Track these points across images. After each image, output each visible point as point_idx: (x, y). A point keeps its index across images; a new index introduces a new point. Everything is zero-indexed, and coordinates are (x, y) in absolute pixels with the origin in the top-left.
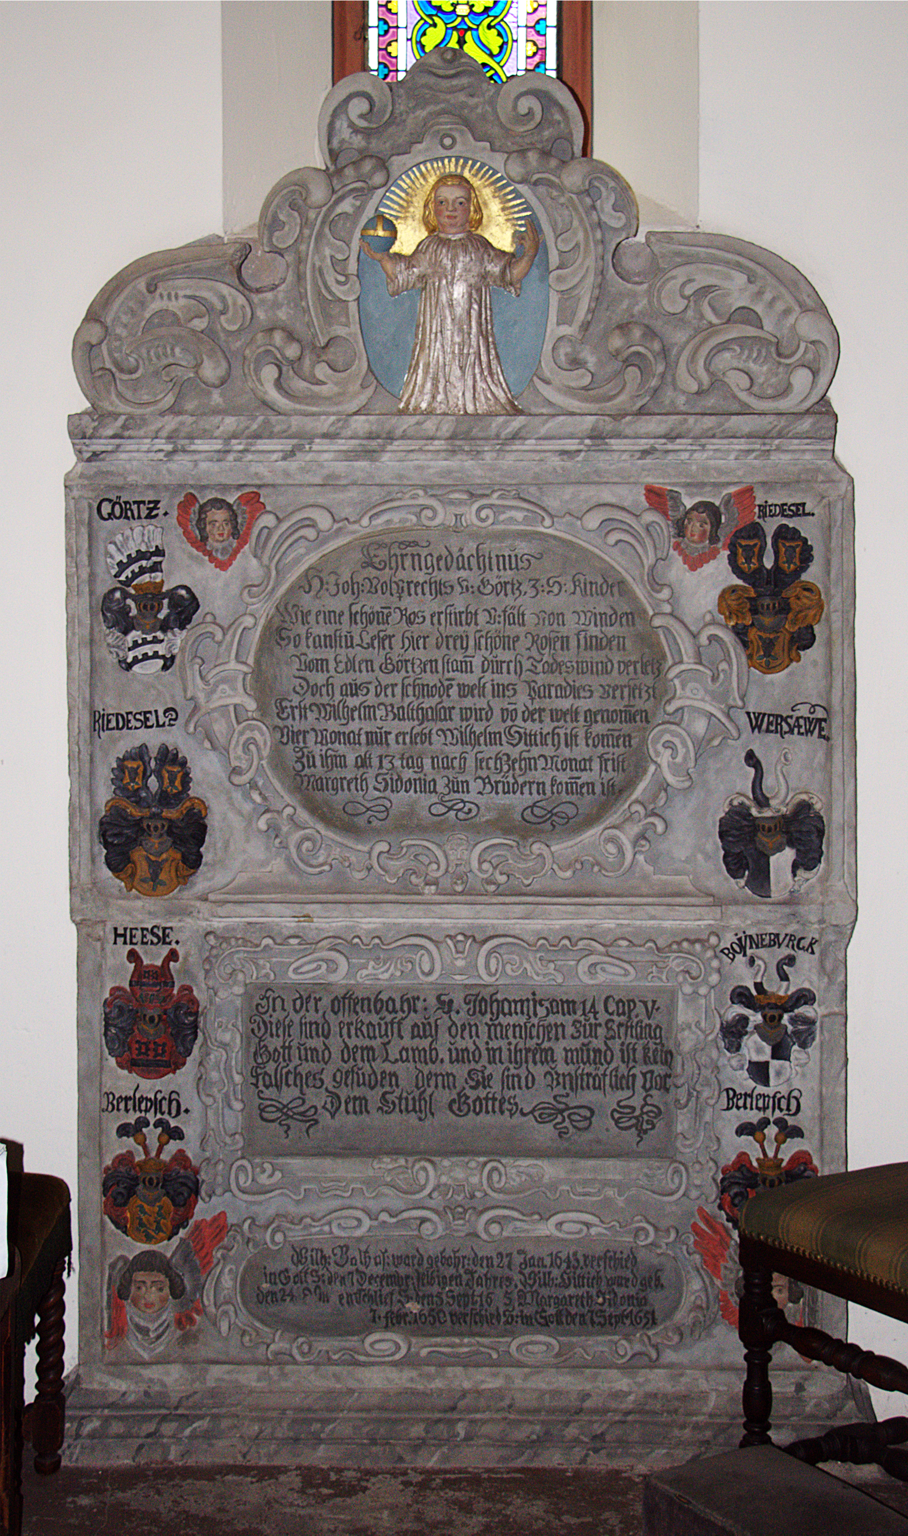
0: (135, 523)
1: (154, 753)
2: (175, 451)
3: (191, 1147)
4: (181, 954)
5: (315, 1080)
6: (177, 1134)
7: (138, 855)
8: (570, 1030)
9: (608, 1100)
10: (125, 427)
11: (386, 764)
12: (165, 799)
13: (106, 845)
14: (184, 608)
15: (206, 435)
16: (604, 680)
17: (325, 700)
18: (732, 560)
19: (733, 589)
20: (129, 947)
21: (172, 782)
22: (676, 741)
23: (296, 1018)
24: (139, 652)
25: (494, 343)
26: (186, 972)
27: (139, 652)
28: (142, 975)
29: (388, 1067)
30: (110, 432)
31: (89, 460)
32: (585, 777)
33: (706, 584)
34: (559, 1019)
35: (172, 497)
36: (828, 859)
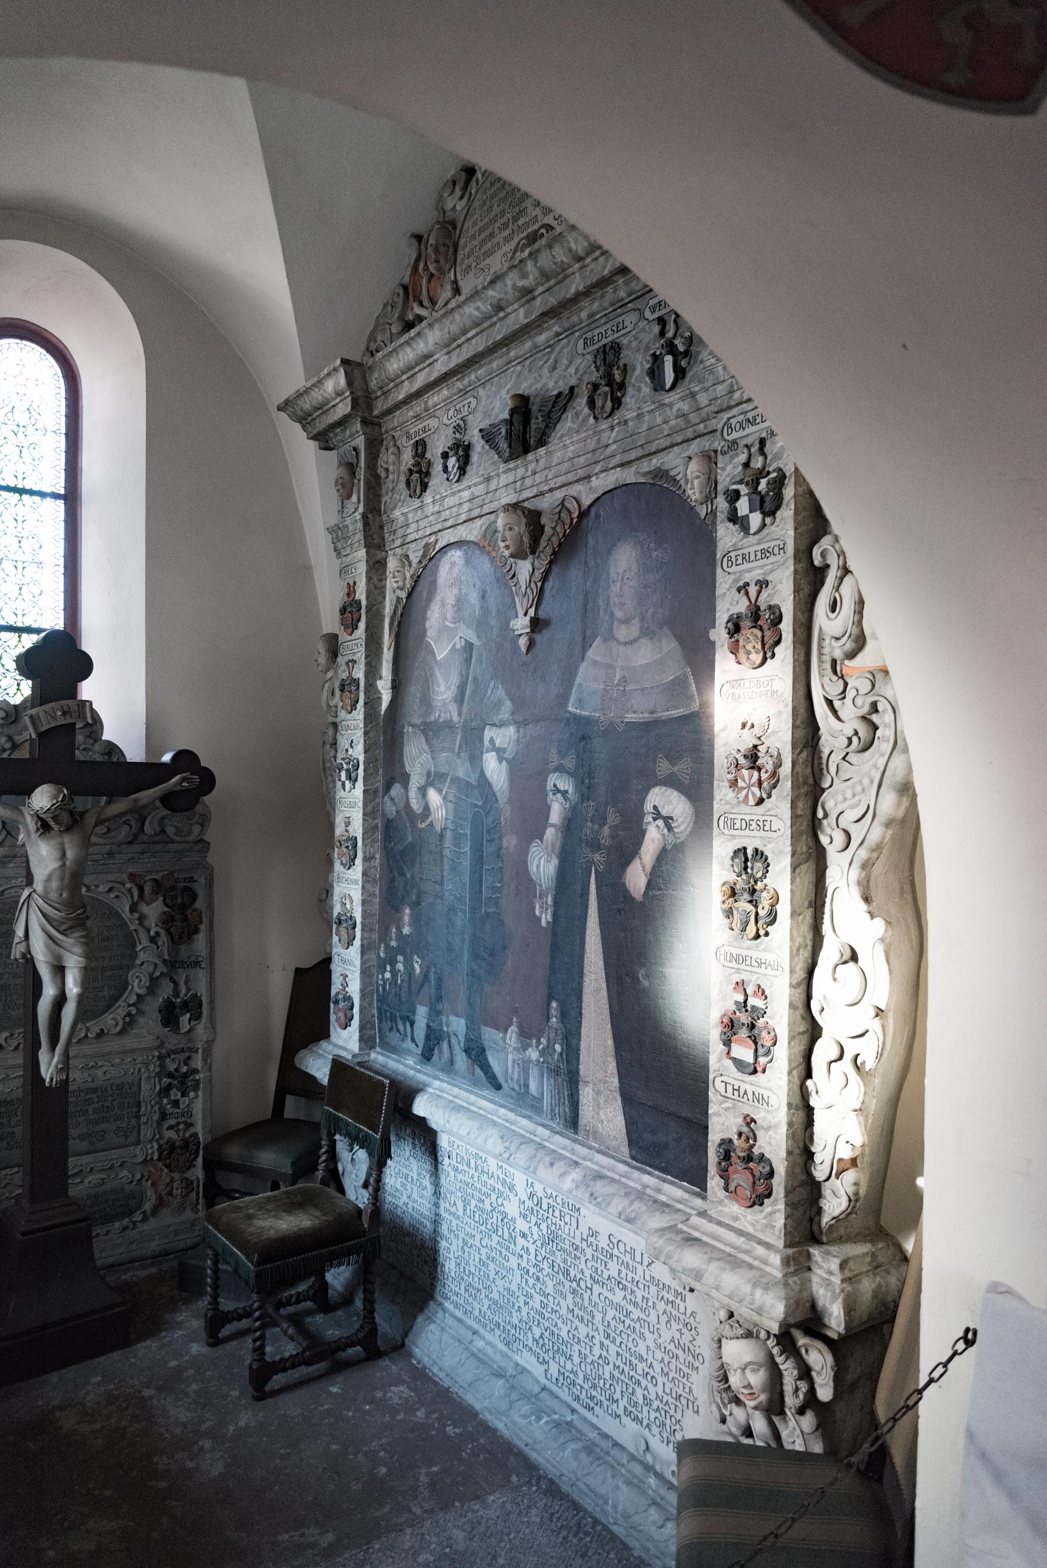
8: (95, 1100)
18: (164, 900)
19: (165, 913)
25: (536, 349)
29: (10, 1130)
32: (101, 994)
33: (154, 911)
34: (90, 1096)
36: (212, 1019)
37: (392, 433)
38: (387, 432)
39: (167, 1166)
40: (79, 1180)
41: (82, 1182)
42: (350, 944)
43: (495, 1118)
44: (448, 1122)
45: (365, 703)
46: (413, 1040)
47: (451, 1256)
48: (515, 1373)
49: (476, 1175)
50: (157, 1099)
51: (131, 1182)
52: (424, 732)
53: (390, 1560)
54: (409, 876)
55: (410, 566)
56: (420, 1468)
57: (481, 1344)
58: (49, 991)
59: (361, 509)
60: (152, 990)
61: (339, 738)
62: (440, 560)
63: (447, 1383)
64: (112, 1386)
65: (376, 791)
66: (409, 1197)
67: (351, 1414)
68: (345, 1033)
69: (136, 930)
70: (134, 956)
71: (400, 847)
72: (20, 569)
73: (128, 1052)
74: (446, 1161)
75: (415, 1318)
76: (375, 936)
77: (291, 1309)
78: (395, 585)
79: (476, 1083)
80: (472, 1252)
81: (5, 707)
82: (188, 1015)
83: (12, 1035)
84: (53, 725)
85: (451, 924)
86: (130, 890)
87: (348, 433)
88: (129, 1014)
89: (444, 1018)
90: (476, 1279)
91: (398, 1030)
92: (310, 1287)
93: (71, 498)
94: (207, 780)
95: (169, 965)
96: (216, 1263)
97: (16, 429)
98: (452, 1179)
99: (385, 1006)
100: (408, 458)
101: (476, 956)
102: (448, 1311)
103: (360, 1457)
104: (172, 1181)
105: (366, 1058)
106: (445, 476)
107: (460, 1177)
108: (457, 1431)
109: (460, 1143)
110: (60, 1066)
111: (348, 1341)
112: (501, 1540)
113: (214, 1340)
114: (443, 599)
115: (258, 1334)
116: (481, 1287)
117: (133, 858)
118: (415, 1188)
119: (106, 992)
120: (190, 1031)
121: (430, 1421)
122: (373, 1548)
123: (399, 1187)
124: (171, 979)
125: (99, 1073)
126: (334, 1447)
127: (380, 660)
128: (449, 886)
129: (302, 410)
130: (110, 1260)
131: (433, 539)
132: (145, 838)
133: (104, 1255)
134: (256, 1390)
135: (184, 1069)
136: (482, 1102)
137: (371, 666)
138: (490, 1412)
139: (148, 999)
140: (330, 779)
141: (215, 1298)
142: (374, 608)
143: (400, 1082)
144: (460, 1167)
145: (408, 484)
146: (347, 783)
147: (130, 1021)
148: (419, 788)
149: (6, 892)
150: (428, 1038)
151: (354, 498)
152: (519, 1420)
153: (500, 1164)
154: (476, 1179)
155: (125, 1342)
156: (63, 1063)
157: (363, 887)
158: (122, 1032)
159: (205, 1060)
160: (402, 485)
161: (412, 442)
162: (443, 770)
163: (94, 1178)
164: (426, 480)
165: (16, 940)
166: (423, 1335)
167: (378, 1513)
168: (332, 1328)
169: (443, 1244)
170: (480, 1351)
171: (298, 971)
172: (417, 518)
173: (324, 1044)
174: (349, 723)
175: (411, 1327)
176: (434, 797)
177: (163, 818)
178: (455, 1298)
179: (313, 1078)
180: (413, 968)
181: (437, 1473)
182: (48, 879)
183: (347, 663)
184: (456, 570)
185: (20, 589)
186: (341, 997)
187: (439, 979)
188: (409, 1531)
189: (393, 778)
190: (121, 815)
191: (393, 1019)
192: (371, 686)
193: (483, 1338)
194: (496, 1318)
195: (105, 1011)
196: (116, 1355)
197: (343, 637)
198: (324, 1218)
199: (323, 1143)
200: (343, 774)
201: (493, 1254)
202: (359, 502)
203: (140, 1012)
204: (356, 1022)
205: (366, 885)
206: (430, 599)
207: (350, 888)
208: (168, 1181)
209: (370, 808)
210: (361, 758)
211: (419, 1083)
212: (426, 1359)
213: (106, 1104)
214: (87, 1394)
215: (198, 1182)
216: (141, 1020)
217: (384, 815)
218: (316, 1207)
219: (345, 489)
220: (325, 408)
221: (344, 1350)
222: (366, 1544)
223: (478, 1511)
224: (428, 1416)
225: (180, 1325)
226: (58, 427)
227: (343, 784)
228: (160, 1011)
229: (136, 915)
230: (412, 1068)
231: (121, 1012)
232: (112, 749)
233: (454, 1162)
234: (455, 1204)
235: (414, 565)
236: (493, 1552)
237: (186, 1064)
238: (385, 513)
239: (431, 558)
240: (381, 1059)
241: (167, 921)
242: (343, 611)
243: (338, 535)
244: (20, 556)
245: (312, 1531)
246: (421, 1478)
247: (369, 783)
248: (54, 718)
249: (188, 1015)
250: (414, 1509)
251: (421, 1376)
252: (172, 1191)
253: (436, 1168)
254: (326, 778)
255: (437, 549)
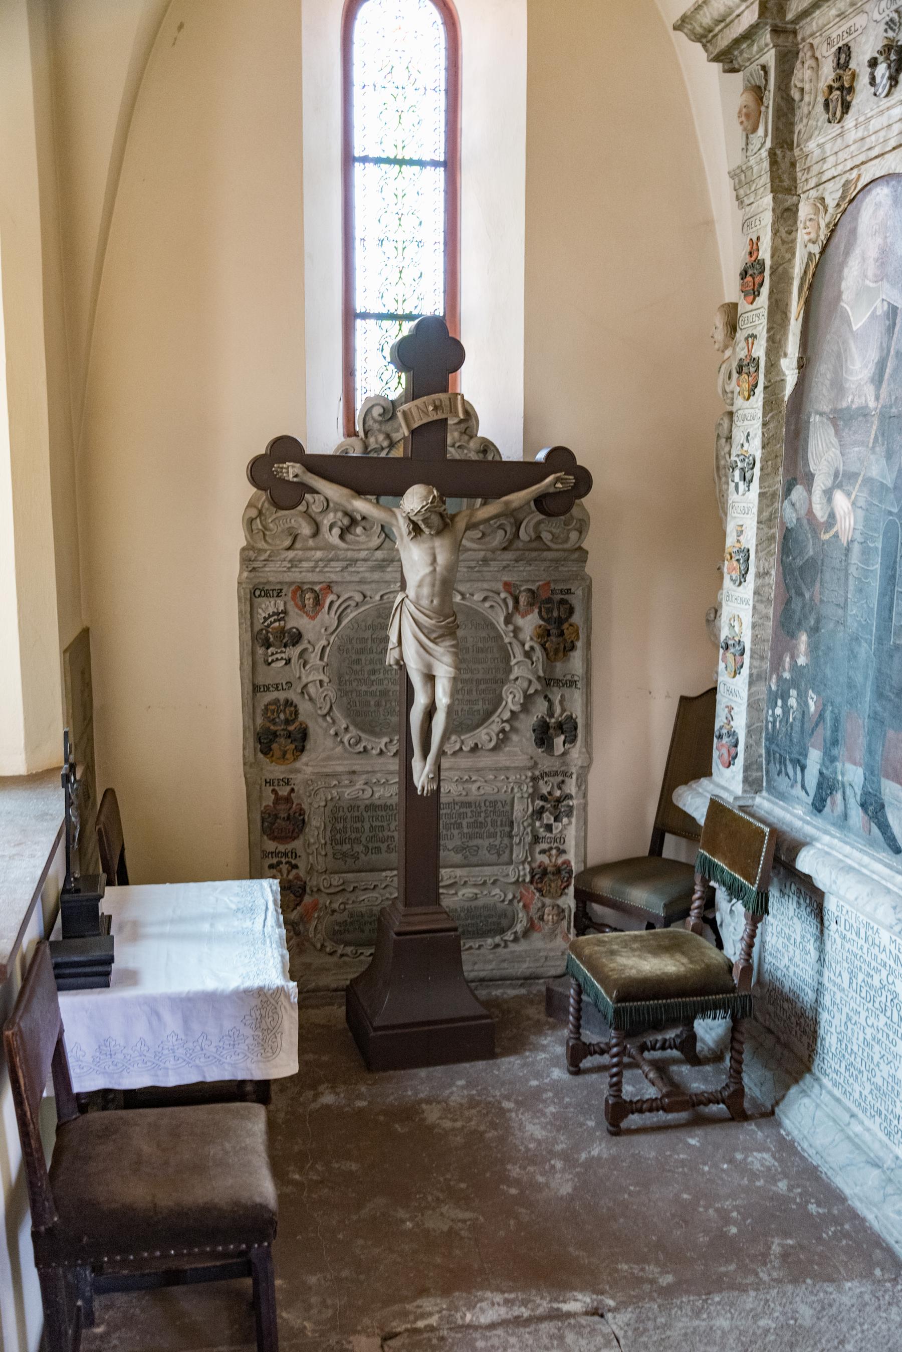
0: (271, 599)
1: (282, 702)
2: (292, 567)
3: (302, 873)
4: (296, 789)
5: (358, 841)
6: (296, 867)
7: (275, 746)
8: (469, 814)
9: (485, 843)
10: (270, 556)
11: (388, 705)
12: (287, 722)
13: (260, 743)
14: (297, 637)
15: (308, 560)
16: (484, 666)
17: (361, 677)
18: (540, 613)
19: (540, 627)
20: (272, 788)
21: (291, 715)
22: (515, 691)
23: (349, 815)
24: (274, 657)
26: (299, 797)
27: (274, 657)
28: (278, 799)
29: (390, 834)
30: (262, 558)
31: (251, 571)
32: (476, 707)
33: (529, 623)
34: (464, 810)
35: (289, 587)
36: (588, 745)
37: (810, 40)
38: (803, 40)
39: (540, 890)
40: (453, 892)
41: (456, 894)
42: (736, 673)
43: (889, 885)
44: (835, 882)
45: (765, 388)
46: (803, 787)
47: (833, 1030)
48: (893, 1166)
49: (866, 946)
50: (530, 821)
51: (503, 901)
52: (834, 422)
53: (729, 1315)
54: (807, 596)
55: (826, 211)
56: (773, 1237)
57: (858, 1129)
58: (421, 700)
59: (768, 144)
60: (526, 707)
61: (735, 431)
62: (862, 201)
63: (816, 1161)
64: (474, 1092)
65: (774, 495)
66: (791, 960)
67: (706, 1168)
68: (727, 772)
69: (510, 643)
70: (509, 670)
71: (799, 562)
72: (400, 250)
73: (501, 769)
74: (833, 927)
75: (788, 1088)
76: (766, 665)
77: (657, 1054)
78: (806, 238)
79: (872, 843)
80: (856, 1029)
81: (382, 403)
82: (562, 737)
83: (391, 741)
84: (425, 421)
85: (853, 655)
86: (505, 600)
87: (755, 48)
88: (503, 731)
89: (839, 765)
90: (859, 1060)
91: (787, 775)
92: (677, 1036)
93: (451, 165)
94: (583, 481)
95: (544, 682)
96: (579, 992)
97: (395, 92)
98: (839, 947)
99: (774, 747)
100: (828, 72)
101: (880, 695)
102: (826, 1088)
103: (711, 1211)
104: (544, 906)
105: (750, 802)
106: (873, 90)
107: (847, 946)
108: (821, 1211)
109: (850, 909)
110: (431, 776)
111: (712, 1097)
112: (853, 1328)
113: (576, 1070)
114: (863, 252)
115: (615, 1070)
116: (863, 1068)
117: (508, 566)
118: (798, 952)
119: (480, 706)
120: (564, 754)
121: (792, 1195)
122: (712, 1299)
123: (780, 948)
124: (546, 697)
125: (474, 787)
126: (685, 1196)
127: (785, 334)
128: (853, 610)
129: (701, 26)
130: (482, 974)
131: (855, 173)
132: (521, 545)
133: (476, 967)
134: (612, 1125)
135: (558, 793)
136: (877, 865)
137: (774, 342)
138: (860, 1200)
139: (522, 716)
140: (723, 479)
141: (578, 1027)
142: (780, 269)
143: (784, 833)
144: (848, 935)
145: (827, 105)
146: (741, 484)
147: (503, 738)
148: (824, 491)
149: (385, 597)
150: (820, 786)
151: (761, 131)
152: (892, 1215)
153: (894, 938)
154: (865, 950)
155: (490, 1055)
156: (434, 774)
157: (754, 607)
158: (495, 749)
159: (579, 786)
160: (820, 108)
161: (834, 49)
162: (853, 469)
163: (468, 892)
164: (848, 98)
165: (390, 646)
166: (796, 1107)
167: (723, 1269)
168: (697, 1081)
169: (824, 1017)
170: (857, 1135)
171: (684, 700)
172: (836, 149)
173: (704, 781)
174: (746, 412)
175: (783, 1097)
176: (841, 502)
177: (539, 523)
178: (835, 1076)
179: (694, 819)
180: (806, 704)
181: (792, 1247)
182: (420, 585)
183: (747, 339)
184: (881, 213)
185: (401, 272)
186: (724, 731)
187: (836, 721)
188: (752, 1293)
189: (795, 479)
190: (496, 516)
191: (782, 761)
192: (772, 365)
193: (862, 1123)
194: (878, 1105)
195: (478, 726)
196: (481, 1064)
197: (744, 306)
198: (691, 966)
199: (697, 888)
200: (737, 473)
201: (880, 1036)
202: (766, 135)
203: (514, 729)
204: (740, 761)
205: (757, 604)
206: (847, 253)
207: (740, 609)
208: (540, 905)
209: (766, 514)
210: (758, 455)
211: (806, 835)
212: (795, 1133)
213: (480, 819)
214: (452, 1093)
215: (570, 911)
216: (515, 738)
217: (783, 523)
218: (683, 953)
219: (750, 120)
220: (728, 20)
221: (706, 1105)
222: (706, 1294)
223: (831, 1293)
224: (790, 1188)
225: (544, 1048)
226: (437, 84)
227: (737, 485)
228: (534, 731)
229: (511, 627)
230: (800, 819)
231: (496, 728)
232: (487, 446)
233: (842, 929)
234: (840, 974)
235: (831, 210)
236: (842, 1337)
237: (560, 788)
238: (798, 145)
239: (851, 200)
240: (766, 805)
241: (543, 635)
242: (744, 274)
243: (741, 178)
244: (400, 237)
245: (652, 1270)
246: (774, 1247)
247: (766, 484)
248: (426, 413)
249: (562, 737)
250: (761, 1275)
251: (787, 1148)
252: (543, 916)
253: (822, 932)
254: (720, 478)
255: (859, 187)
